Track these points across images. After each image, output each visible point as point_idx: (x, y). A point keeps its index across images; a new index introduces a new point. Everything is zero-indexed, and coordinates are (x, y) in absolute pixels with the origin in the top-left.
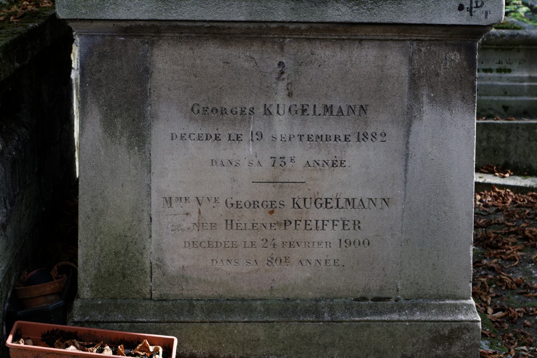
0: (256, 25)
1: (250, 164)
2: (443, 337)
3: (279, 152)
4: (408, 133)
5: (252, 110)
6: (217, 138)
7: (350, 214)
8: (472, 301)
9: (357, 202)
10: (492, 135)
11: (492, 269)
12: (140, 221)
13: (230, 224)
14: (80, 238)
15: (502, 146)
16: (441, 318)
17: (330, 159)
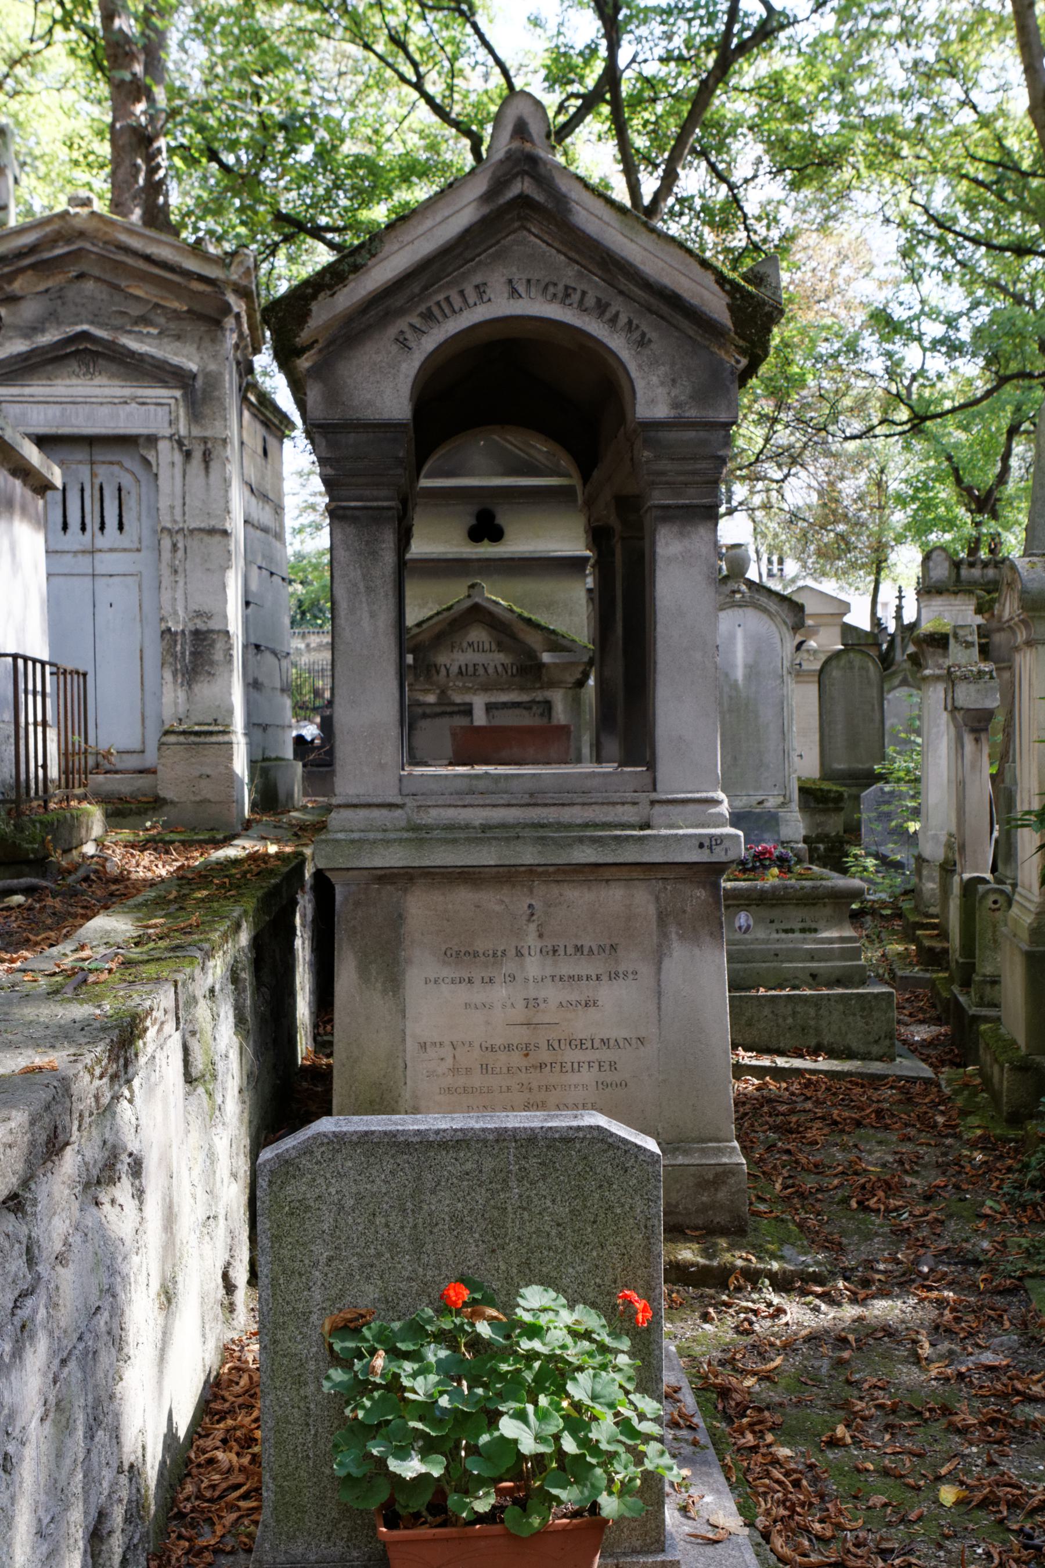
0: (506, 869)
1: (504, 1006)
2: (708, 1182)
3: (532, 993)
4: (659, 970)
5: (504, 952)
6: (470, 981)
7: (606, 1055)
8: (736, 1144)
9: (612, 1042)
10: (798, 1009)
11: (788, 1152)
12: (395, 1068)
13: (485, 1068)
14: (335, 1086)
15: (812, 1023)
16: (704, 1161)
17: (583, 999)
